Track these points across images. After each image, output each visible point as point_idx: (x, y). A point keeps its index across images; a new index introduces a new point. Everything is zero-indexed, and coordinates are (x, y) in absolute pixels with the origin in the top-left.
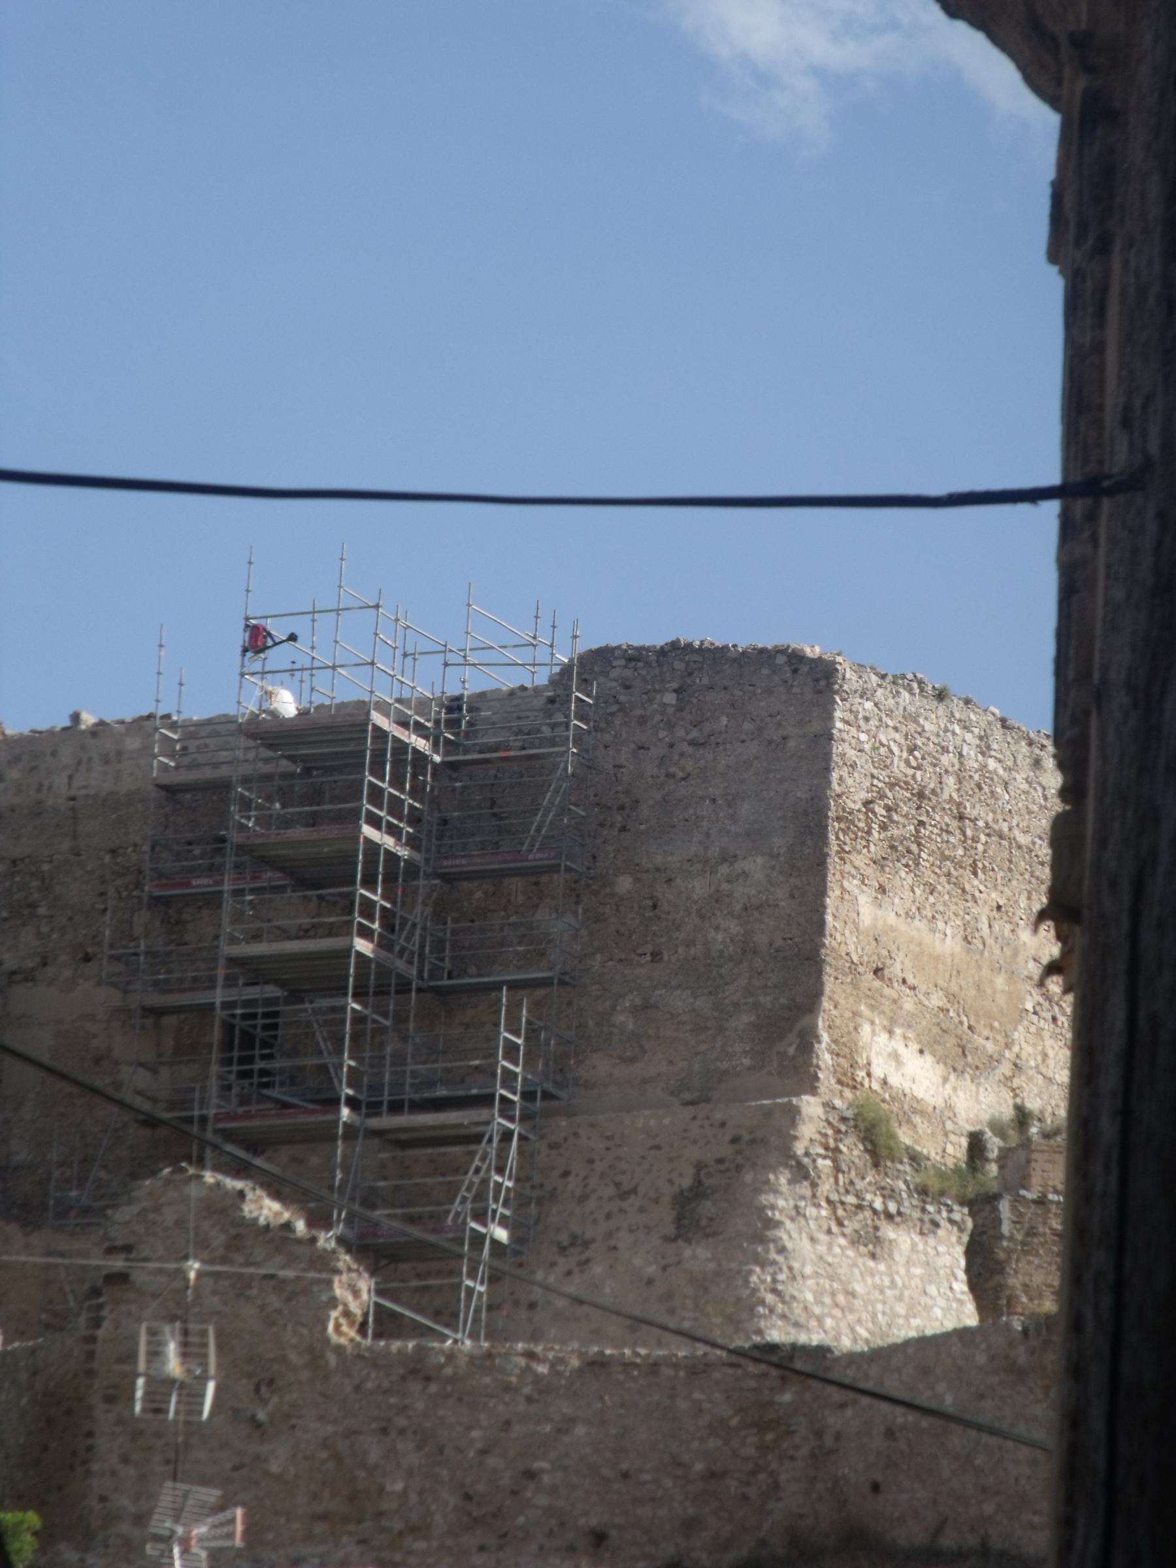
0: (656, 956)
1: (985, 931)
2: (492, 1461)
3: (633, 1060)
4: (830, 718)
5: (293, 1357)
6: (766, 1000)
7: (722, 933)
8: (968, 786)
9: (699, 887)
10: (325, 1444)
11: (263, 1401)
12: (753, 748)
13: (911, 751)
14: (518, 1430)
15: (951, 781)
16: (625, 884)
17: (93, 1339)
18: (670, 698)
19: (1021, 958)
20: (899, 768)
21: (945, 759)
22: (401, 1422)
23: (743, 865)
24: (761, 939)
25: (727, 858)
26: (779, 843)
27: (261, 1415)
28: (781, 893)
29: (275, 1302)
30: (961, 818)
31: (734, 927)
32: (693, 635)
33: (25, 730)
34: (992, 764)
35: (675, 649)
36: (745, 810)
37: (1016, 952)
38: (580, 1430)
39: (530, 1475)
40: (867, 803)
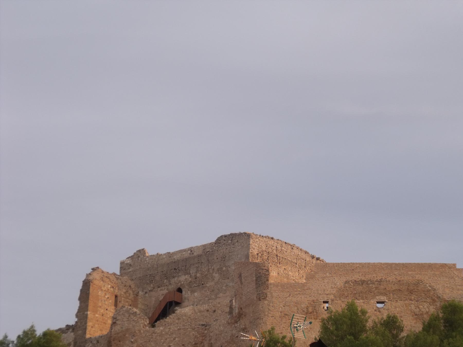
0: (228, 278)
1: (282, 272)
2: (165, 344)
3: (225, 293)
4: (249, 242)
5: (137, 332)
8: (278, 252)
10: (141, 344)
11: (133, 338)
12: (240, 247)
13: (267, 246)
14: (168, 340)
15: (275, 251)
16: (224, 268)
17: (111, 332)
18: (230, 241)
19: (290, 276)
20: (264, 248)
21: (274, 248)
22: (152, 340)
27: (132, 340)
29: (134, 324)
30: (277, 256)
32: (234, 232)
33: (154, 253)
34: (283, 249)
35: (231, 234)
36: (239, 256)
37: (288, 275)
38: (177, 339)
40: (257, 254)
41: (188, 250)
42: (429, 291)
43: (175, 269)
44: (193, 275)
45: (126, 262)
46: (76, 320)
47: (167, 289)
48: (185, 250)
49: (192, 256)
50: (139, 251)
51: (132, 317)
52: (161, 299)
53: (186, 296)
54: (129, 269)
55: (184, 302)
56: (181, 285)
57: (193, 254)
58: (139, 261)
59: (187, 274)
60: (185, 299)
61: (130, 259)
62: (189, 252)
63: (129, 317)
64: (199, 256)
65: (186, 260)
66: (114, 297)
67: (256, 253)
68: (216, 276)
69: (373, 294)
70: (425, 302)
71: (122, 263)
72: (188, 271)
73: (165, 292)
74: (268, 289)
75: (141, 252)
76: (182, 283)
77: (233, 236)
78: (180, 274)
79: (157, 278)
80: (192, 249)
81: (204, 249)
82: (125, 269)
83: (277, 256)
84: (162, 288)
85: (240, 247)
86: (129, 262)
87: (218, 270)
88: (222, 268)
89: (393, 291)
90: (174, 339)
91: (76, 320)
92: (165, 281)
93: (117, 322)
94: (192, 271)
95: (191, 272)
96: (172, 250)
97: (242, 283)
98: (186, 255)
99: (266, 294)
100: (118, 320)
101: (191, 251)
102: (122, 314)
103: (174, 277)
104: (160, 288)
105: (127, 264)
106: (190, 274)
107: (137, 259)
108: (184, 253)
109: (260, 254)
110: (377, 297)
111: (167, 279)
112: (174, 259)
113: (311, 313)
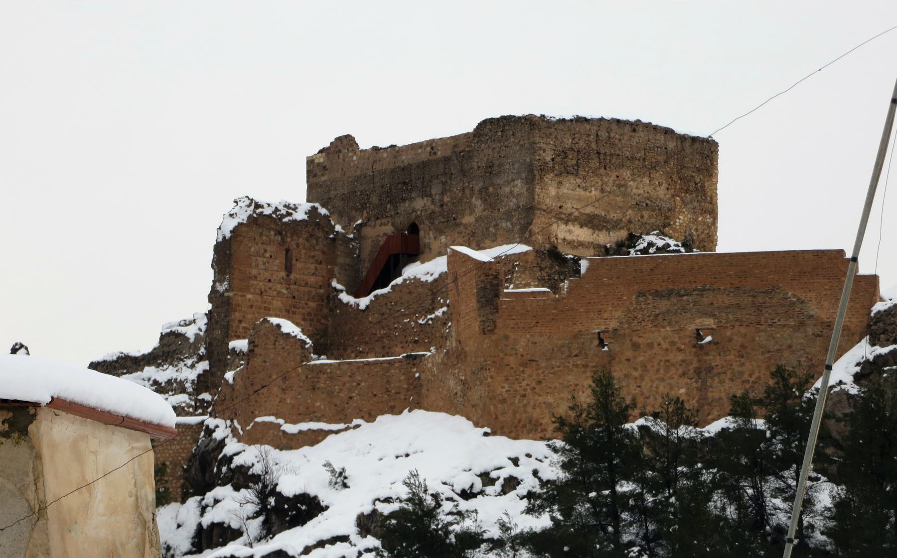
6: (522, 221)
7: (512, 204)
9: (507, 189)
16: (491, 189)
17: (140, 514)
18: (500, 134)
23: (516, 182)
24: (521, 204)
25: (513, 180)
26: (524, 175)
28: (525, 190)
30: (598, 153)
31: (515, 200)
35: (503, 118)
36: (516, 166)
38: (363, 384)
39: (351, 398)
41: (427, 145)
42: (792, 304)
43: (405, 183)
44: (437, 197)
45: (317, 161)
46: (211, 305)
47: (393, 225)
48: (419, 145)
49: (434, 157)
50: (339, 139)
51: (282, 342)
52: (381, 243)
53: (427, 241)
54: (323, 175)
55: (423, 253)
56: (417, 217)
57: (435, 153)
58: (341, 161)
59: (427, 196)
60: (425, 245)
61: (324, 154)
62: (429, 149)
63: (276, 341)
64: (447, 160)
65: (424, 166)
66: (285, 252)
67: (548, 159)
68: (477, 202)
69: (688, 315)
70: (785, 325)
71: (310, 162)
72: (428, 189)
73: (389, 229)
74: (497, 312)
75: (345, 143)
76: (419, 213)
77: (507, 120)
78: (413, 195)
79: (374, 199)
80: (434, 145)
81: (455, 146)
82: (315, 176)
83: (598, 153)
84: (384, 221)
85: (518, 147)
86: (322, 160)
87: (480, 191)
88: (487, 188)
89: (727, 308)
90: (359, 384)
91: (210, 307)
92: (389, 206)
93: (256, 350)
94: (436, 190)
95: (433, 192)
96: (401, 141)
97: (459, 294)
98: (424, 156)
99: (494, 322)
100: (257, 346)
101: (432, 148)
102: (265, 334)
103: (404, 200)
104: (379, 222)
105: (319, 164)
106: (431, 196)
107: (336, 157)
108: (420, 151)
109: (558, 159)
110: (698, 321)
111: (390, 202)
112: (403, 161)
113: (576, 356)
